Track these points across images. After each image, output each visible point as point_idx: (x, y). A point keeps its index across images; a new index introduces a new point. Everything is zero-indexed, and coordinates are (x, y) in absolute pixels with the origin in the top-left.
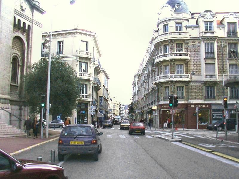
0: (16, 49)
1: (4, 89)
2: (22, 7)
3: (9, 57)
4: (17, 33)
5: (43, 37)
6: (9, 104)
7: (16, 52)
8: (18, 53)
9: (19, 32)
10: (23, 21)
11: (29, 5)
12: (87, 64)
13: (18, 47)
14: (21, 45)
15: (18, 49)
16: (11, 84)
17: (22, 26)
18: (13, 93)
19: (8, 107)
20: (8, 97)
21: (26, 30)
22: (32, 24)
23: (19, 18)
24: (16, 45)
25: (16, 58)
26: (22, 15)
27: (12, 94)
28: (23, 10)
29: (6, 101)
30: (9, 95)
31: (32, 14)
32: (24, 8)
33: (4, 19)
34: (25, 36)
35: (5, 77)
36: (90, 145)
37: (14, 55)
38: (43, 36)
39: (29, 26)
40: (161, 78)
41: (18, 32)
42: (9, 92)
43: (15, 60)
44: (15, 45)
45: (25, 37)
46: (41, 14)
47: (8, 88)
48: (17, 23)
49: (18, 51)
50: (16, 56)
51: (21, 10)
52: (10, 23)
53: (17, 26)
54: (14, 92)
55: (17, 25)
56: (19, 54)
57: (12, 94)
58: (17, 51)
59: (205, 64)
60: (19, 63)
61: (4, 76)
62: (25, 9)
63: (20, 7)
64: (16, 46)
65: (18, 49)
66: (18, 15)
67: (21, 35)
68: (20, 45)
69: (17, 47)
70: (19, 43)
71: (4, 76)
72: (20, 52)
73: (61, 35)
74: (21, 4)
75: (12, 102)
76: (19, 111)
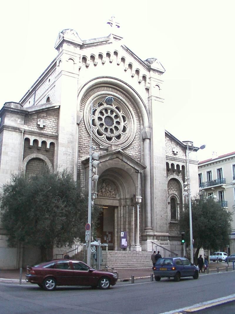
0: (173, 189)
1: (162, 228)
2: (174, 152)
3: (165, 200)
4: (172, 175)
5: (200, 168)
6: (168, 241)
7: (174, 193)
8: (175, 193)
9: (175, 174)
10: (176, 164)
11: (181, 147)
12: (141, 174)
13: (174, 187)
14: (178, 185)
15: (175, 190)
16: (171, 222)
17: (175, 168)
18: (174, 230)
19: (167, 243)
20: (167, 234)
21: (182, 171)
22: (186, 164)
23: (172, 163)
24: (173, 186)
25: (174, 197)
26: (174, 159)
27: (173, 230)
28: (175, 154)
29: (166, 238)
30: (167, 232)
31: (185, 155)
32: (175, 153)
33: (157, 168)
34: (181, 176)
35: (163, 217)
36: (170, 271)
37: (171, 195)
38: (199, 167)
39: (183, 167)
40: (51, 137)
41: (173, 174)
42: (168, 229)
43: (173, 199)
44: (172, 187)
45: (181, 177)
46: (205, 148)
47: (166, 227)
48: (170, 167)
49: (175, 191)
50: (173, 196)
51: (173, 154)
52: (163, 169)
53: (170, 169)
54: (174, 229)
55: (170, 169)
56: (177, 194)
57: (173, 230)
58: (174, 191)
59: (56, 49)
60: (177, 202)
61: (161, 216)
62: (177, 152)
63: (172, 152)
64: (173, 187)
65: (175, 190)
66: (171, 160)
67: (176, 177)
68: (177, 185)
69: (174, 188)
70: (176, 183)
71: (161, 216)
72: (177, 192)
73: (232, 159)
74: (172, 150)
75: (171, 238)
76: (181, 246)
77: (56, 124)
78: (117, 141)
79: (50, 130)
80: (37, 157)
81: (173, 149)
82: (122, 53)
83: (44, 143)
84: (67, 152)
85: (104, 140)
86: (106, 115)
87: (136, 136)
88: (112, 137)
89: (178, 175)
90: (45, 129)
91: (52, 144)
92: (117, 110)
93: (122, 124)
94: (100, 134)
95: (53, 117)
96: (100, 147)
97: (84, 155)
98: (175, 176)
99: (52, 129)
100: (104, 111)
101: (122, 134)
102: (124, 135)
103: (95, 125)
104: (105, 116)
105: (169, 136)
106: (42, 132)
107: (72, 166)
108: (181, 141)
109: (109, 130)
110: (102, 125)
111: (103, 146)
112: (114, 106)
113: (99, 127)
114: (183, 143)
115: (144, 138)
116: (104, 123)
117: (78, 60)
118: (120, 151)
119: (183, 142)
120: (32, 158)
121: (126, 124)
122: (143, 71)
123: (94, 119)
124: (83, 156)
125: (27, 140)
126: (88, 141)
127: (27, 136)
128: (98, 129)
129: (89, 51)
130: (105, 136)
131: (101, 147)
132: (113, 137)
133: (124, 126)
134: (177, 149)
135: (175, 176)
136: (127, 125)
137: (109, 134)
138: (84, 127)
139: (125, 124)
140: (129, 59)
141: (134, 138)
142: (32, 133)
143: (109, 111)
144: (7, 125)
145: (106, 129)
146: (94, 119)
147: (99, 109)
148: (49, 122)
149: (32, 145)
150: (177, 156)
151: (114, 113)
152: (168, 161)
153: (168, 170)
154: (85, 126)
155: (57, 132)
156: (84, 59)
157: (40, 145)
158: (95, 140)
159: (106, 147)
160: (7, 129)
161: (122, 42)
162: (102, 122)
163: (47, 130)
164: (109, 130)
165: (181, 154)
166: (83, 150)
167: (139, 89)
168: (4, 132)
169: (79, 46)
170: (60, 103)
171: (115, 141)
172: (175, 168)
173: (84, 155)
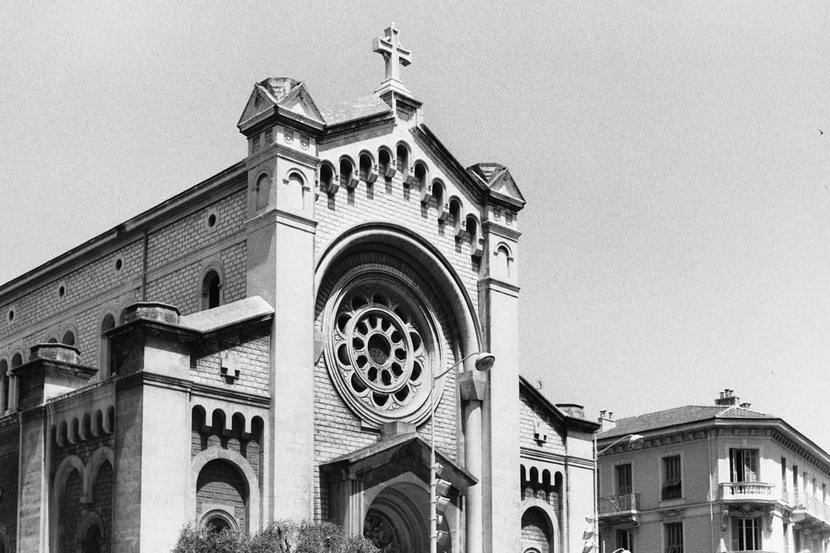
10: (230, 410)
17: (540, 480)
39: (558, 475)
51: (535, 443)
62: (545, 437)
77: (263, 364)
78: (398, 407)
79: (250, 384)
80: (222, 457)
81: (537, 428)
82: (417, 153)
83: (238, 419)
84: (295, 443)
85: (367, 403)
86: (371, 332)
87: (446, 393)
88: (388, 396)
89: (548, 500)
90: (238, 379)
91: (257, 422)
92: (399, 317)
93: (412, 356)
94: (359, 387)
95: (255, 347)
96: (362, 426)
97: (325, 447)
98: (540, 503)
99: (256, 381)
100: (366, 322)
101: (410, 384)
102: (414, 389)
103: (346, 362)
104: (368, 336)
105: (530, 395)
106: (232, 388)
107: (307, 480)
108: (553, 402)
109: (379, 375)
110: (362, 361)
111: (370, 422)
112: (392, 305)
113: (357, 367)
114: (560, 410)
115: (467, 398)
116: (368, 356)
117: (312, 176)
118: (417, 438)
119: (558, 406)
120: (209, 460)
121: (421, 356)
122: (468, 208)
123: (345, 345)
124: (323, 449)
125: (198, 413)
126: (332, 408)
127: (197, 401)
128: (353, 371)
129: (345, 148)
130: (372, 392)
131: (364, 425)
132: (390, 395)
133: (415, 362)
134: (545, 429)
135: (540, 503)
136: (422, 359)
137: (378, 385)
138: (325, 370)
139: (417, 357)
140: (435, 172)
141: (441, 399)
142: (208, 391)
143: (379, 321)
144: (152, 372)
145: (372, 374)
146: (345, 345)
147: (355, 315)
148: (248, 361)
149: (211, 425)
150: (544, 449)
151: (392, 326)
152: (529, 465)
153: (524, 485)
154: (327, 368)
155: (271, 383)
156: (326, 170)
157: (229, 425)
158: (350, 405)
159: (377, 426)
160: (265, 406)
161: (418, 119)
162: (363, 353)
163: (245, 383)
164: (379, 375)
165: (553, 442)
166: (323, 434)
167: (460, 260)
168: (145, 392)
169: (314, 134)
170: (274, 305)
171: (394, 405)
172: (540, 480)
173: (325, 447)
